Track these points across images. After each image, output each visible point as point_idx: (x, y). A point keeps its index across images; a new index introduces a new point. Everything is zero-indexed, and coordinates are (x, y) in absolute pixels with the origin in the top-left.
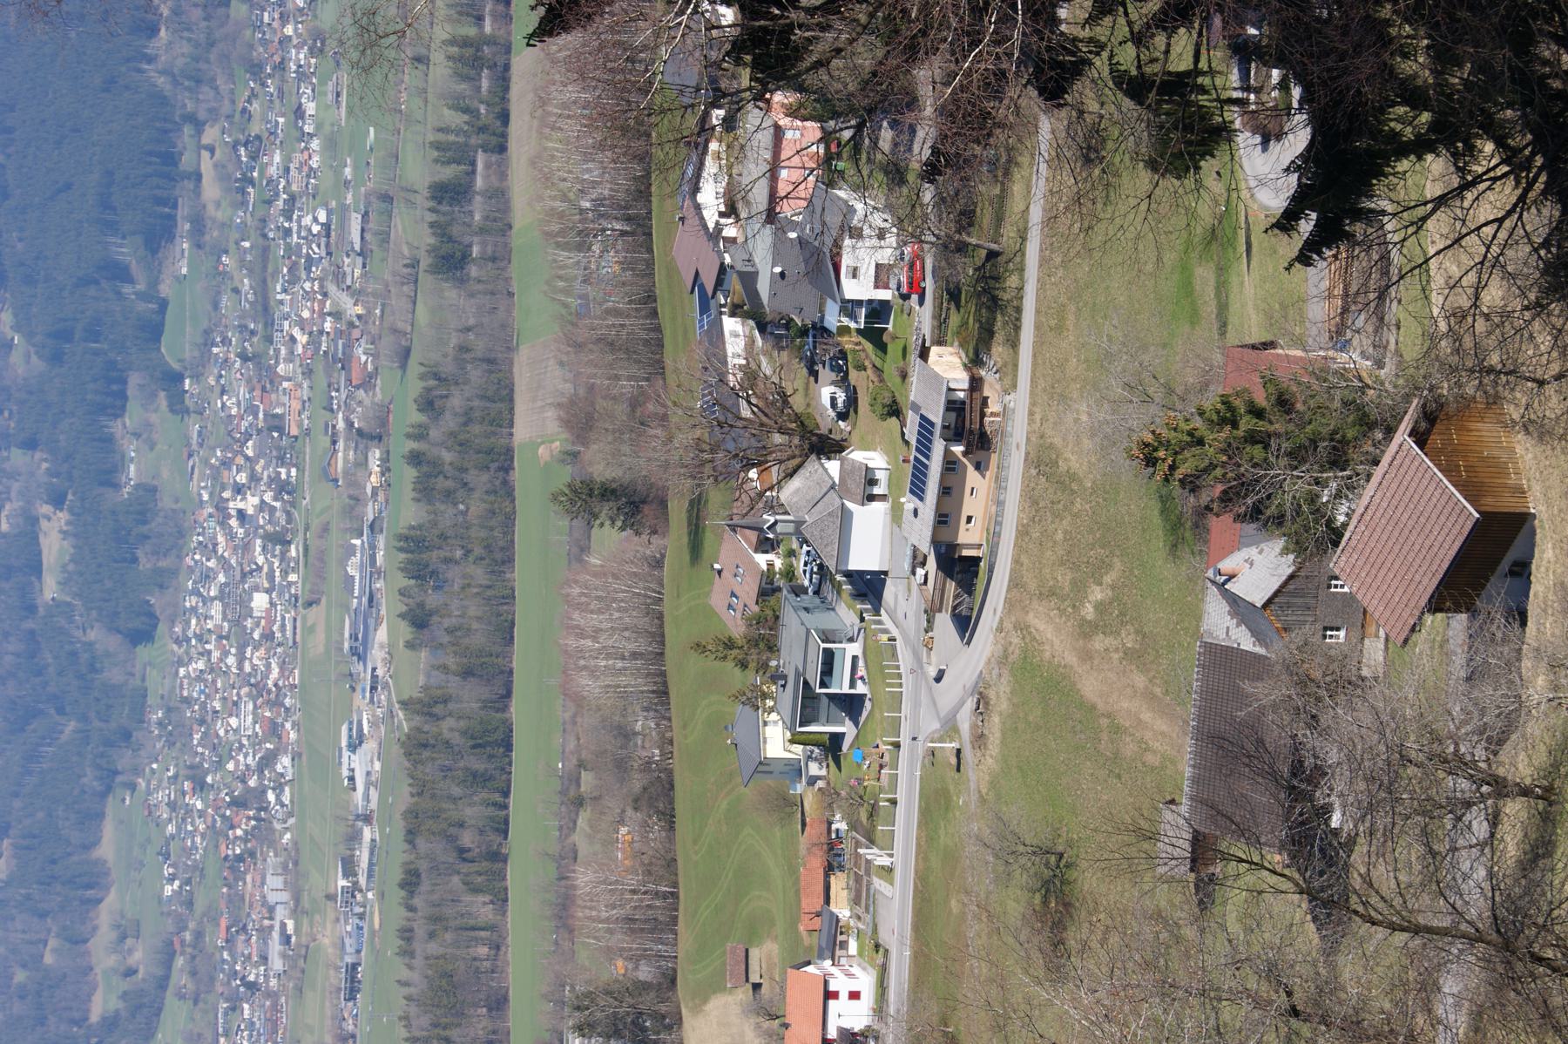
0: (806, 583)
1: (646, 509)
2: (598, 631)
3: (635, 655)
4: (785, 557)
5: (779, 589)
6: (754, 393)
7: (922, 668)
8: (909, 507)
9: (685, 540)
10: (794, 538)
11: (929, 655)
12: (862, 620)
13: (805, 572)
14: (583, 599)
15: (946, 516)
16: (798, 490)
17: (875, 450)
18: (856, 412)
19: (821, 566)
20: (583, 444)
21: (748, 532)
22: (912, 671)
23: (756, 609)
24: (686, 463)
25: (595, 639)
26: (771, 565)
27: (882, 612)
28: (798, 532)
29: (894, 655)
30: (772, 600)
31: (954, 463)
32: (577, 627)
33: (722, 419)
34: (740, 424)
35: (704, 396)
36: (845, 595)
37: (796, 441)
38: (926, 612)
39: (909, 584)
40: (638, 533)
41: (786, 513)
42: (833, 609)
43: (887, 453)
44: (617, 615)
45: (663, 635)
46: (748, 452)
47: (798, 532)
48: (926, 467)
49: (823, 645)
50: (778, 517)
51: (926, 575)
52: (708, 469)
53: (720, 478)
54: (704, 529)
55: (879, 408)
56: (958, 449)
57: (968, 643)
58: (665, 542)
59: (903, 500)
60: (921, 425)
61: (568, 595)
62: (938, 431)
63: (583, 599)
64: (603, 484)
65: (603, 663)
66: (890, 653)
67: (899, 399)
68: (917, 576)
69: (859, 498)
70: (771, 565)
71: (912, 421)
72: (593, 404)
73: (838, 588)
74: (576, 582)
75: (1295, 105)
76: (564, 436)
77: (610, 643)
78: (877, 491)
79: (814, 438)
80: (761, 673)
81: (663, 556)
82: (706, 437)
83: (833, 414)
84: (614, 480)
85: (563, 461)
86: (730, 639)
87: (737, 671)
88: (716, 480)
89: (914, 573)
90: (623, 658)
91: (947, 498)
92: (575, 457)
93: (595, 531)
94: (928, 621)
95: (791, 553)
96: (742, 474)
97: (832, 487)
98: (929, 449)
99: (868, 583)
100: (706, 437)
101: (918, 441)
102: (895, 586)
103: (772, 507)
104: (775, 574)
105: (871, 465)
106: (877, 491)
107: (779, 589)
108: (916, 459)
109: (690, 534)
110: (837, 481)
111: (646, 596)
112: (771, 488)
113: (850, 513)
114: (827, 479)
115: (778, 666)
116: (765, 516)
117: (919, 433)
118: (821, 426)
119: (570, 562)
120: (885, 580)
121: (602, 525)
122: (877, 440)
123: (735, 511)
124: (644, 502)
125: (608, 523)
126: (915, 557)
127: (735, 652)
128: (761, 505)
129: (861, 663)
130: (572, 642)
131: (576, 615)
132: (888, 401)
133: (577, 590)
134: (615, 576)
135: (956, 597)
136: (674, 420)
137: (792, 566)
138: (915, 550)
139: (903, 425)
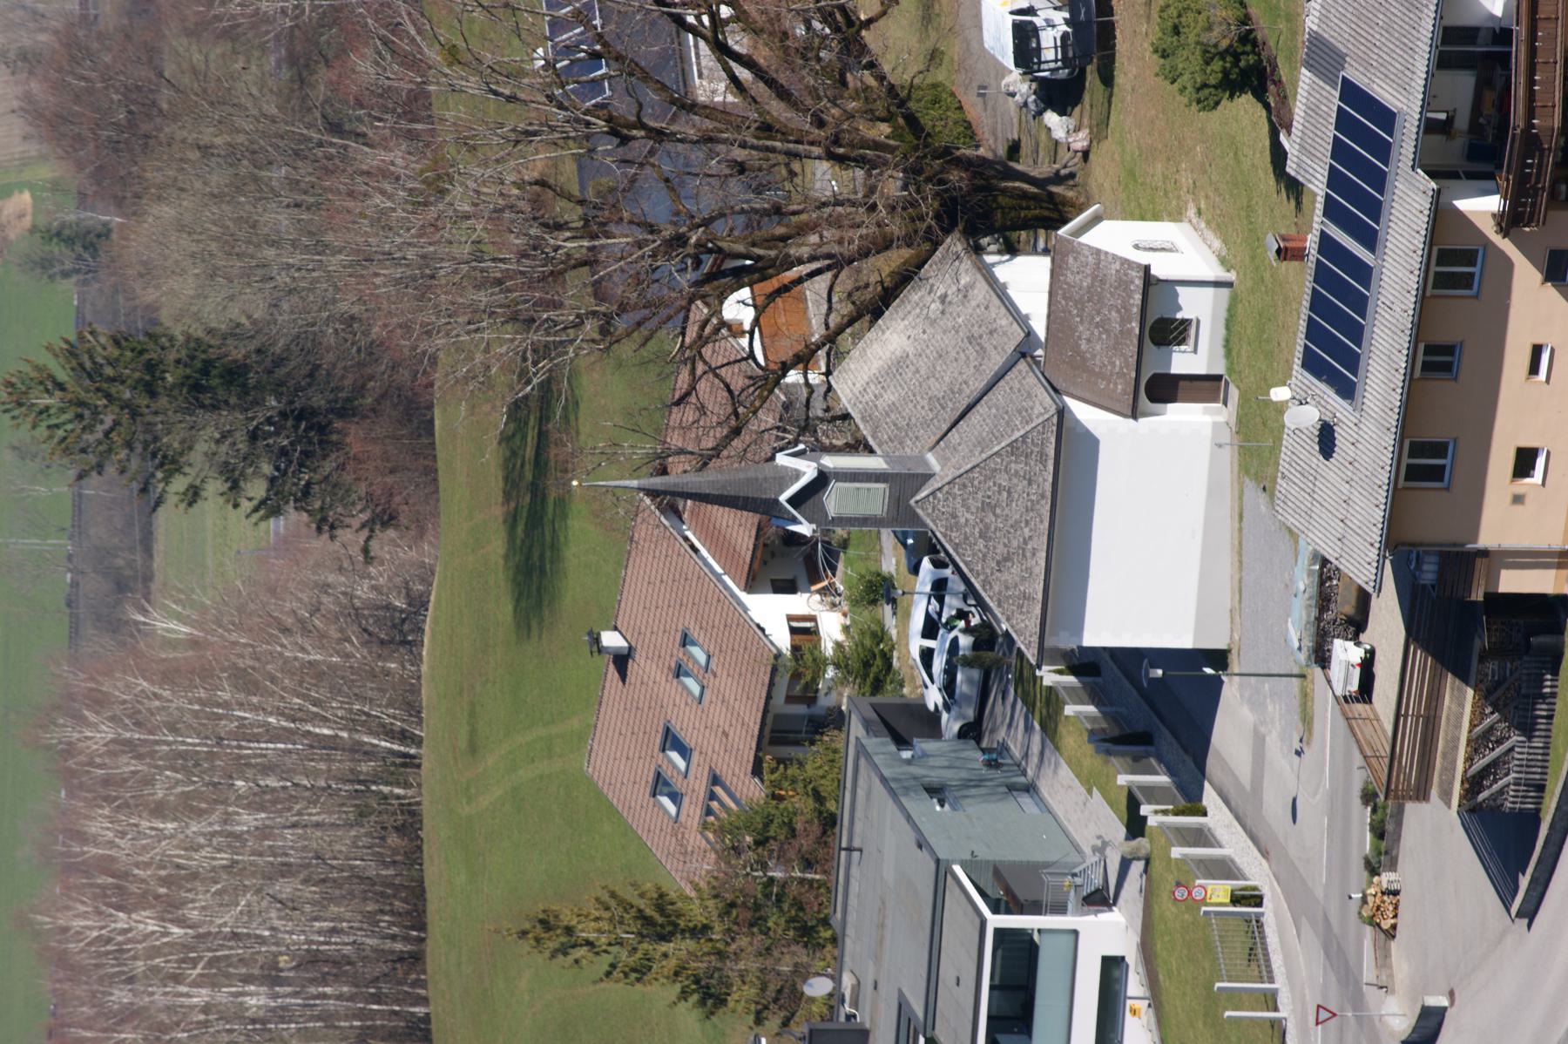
0: (934, 697)
1: (354, 435)
2: (181, 879)
3: (313, 962)
4: (855, 603)
5: (837, 719)
6: (740, 16)
7: (1357, 1000)
8: (1305, 418)
9: (497, 546)
10: (887, 538)
11: (1383, 958)
12: (1136, 826)
13: (927, 655)
14: (127, 765)
15: (1439, 449)
16: (900, 364)
17: (1176, 216)
18: (1107, 79)
19: (986, 637)
20: (119, 202)
21: (724, 517)
22: (1323, 1014)
23: (753, 791)
24: (496, 270)
25: (170, 909)
26: (803, 631)
27: (1210, 797)
28: (901, 515)
29: (1256, 954)
30: (812, 759)
31: (1469, 257)
32: (106, 865)
33: (624, 108)
34: (689, 127)
35: (557, 25)
36: (1073, 740)
37: (892, 185)
38: (1368, 797)
39: (1305, 696)
40: (325, 524)
41: (859, 446)
42: (1030, 789)
43: (1219, 222)
44: (247, 820)
45: (418, 893)
46: (720, 228)
47: (901, 515)
48: (1364, 273)
49: (996, 921)
50: (830, 462)
51: (1367, 666)
52: (575, 292)
53: (621, 325)
54: (563, 503)
55: (1189, 62)
56: (1482, 206)
57: (1529, 913)
58: (426, 552)
59: (1280, 394)
60: (1343, 121)
61: (70, 750)
62: (1406, 141)
63: (127, 765)
64: (195, 346)
65: (201, 996)
66: (1240, 945)
67: (1264, 27)
68: (1336, 671)
69: (1122, 387)
70: (803, 631)
71: (1312, 109)
72: (151, 54)
73: (1047, 710)
74: (99, 701)
75: (357, 736)
76: (45, 173)
77: (227, 920)
78: (1183, 362)
79: (955, 176)
80: (773, 1023)
81: (419, 604)
82: (568, 175)
83: (1017, 83)
84: (235, 332)
85: (45, 264)
86: (661, 901)
87: (688, 1015)
88: (604, 331)
89: (1322, 658)
90: (271, 977)
91: (1440, 387)
92: (91, 247)
93: (169, 518)
94: (1379, 832)
95: (879, 591)
96: (700, 310)
97: (1024, 352)
98: (1375, 209)
99: (1153, 695)
100: (568, 175)
101: (1334, 179)
102: (1257, 705)
103: (807, 427)
104: (820, 664)
105: (1162, 268)
106: (1183, 362)
107: (837, 719)
108: (1326, 243)
109: (511, 521)
110: (1039, 327)
111: (358, 750)
112: (803, 359)
113: (1090, 444)
114: (1005, 321)
115: (835, 998)
116: (782, 459)
117: (1339, 150)
118: (984, 133)
119: (75, 631)
120: (1215, 686)
121: (193, 495)
122: (1186, 180)
123: (675, 440)
124: (345, 411)
125: (214, 487)
126: (1324, 599)
127: (678, 948)
128: (767, 418)
129: (1135, 985)
130: (83, 921)
131: (99, 824)
132: (1222, 37)
133: (104, 733)
134: (245, 681)
135: (1478, 743)
136: (453, 112)
137: (880, 635)
138: (1325, 572)
139: (1279, 123)
